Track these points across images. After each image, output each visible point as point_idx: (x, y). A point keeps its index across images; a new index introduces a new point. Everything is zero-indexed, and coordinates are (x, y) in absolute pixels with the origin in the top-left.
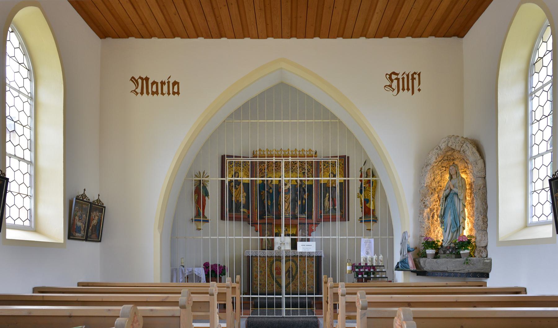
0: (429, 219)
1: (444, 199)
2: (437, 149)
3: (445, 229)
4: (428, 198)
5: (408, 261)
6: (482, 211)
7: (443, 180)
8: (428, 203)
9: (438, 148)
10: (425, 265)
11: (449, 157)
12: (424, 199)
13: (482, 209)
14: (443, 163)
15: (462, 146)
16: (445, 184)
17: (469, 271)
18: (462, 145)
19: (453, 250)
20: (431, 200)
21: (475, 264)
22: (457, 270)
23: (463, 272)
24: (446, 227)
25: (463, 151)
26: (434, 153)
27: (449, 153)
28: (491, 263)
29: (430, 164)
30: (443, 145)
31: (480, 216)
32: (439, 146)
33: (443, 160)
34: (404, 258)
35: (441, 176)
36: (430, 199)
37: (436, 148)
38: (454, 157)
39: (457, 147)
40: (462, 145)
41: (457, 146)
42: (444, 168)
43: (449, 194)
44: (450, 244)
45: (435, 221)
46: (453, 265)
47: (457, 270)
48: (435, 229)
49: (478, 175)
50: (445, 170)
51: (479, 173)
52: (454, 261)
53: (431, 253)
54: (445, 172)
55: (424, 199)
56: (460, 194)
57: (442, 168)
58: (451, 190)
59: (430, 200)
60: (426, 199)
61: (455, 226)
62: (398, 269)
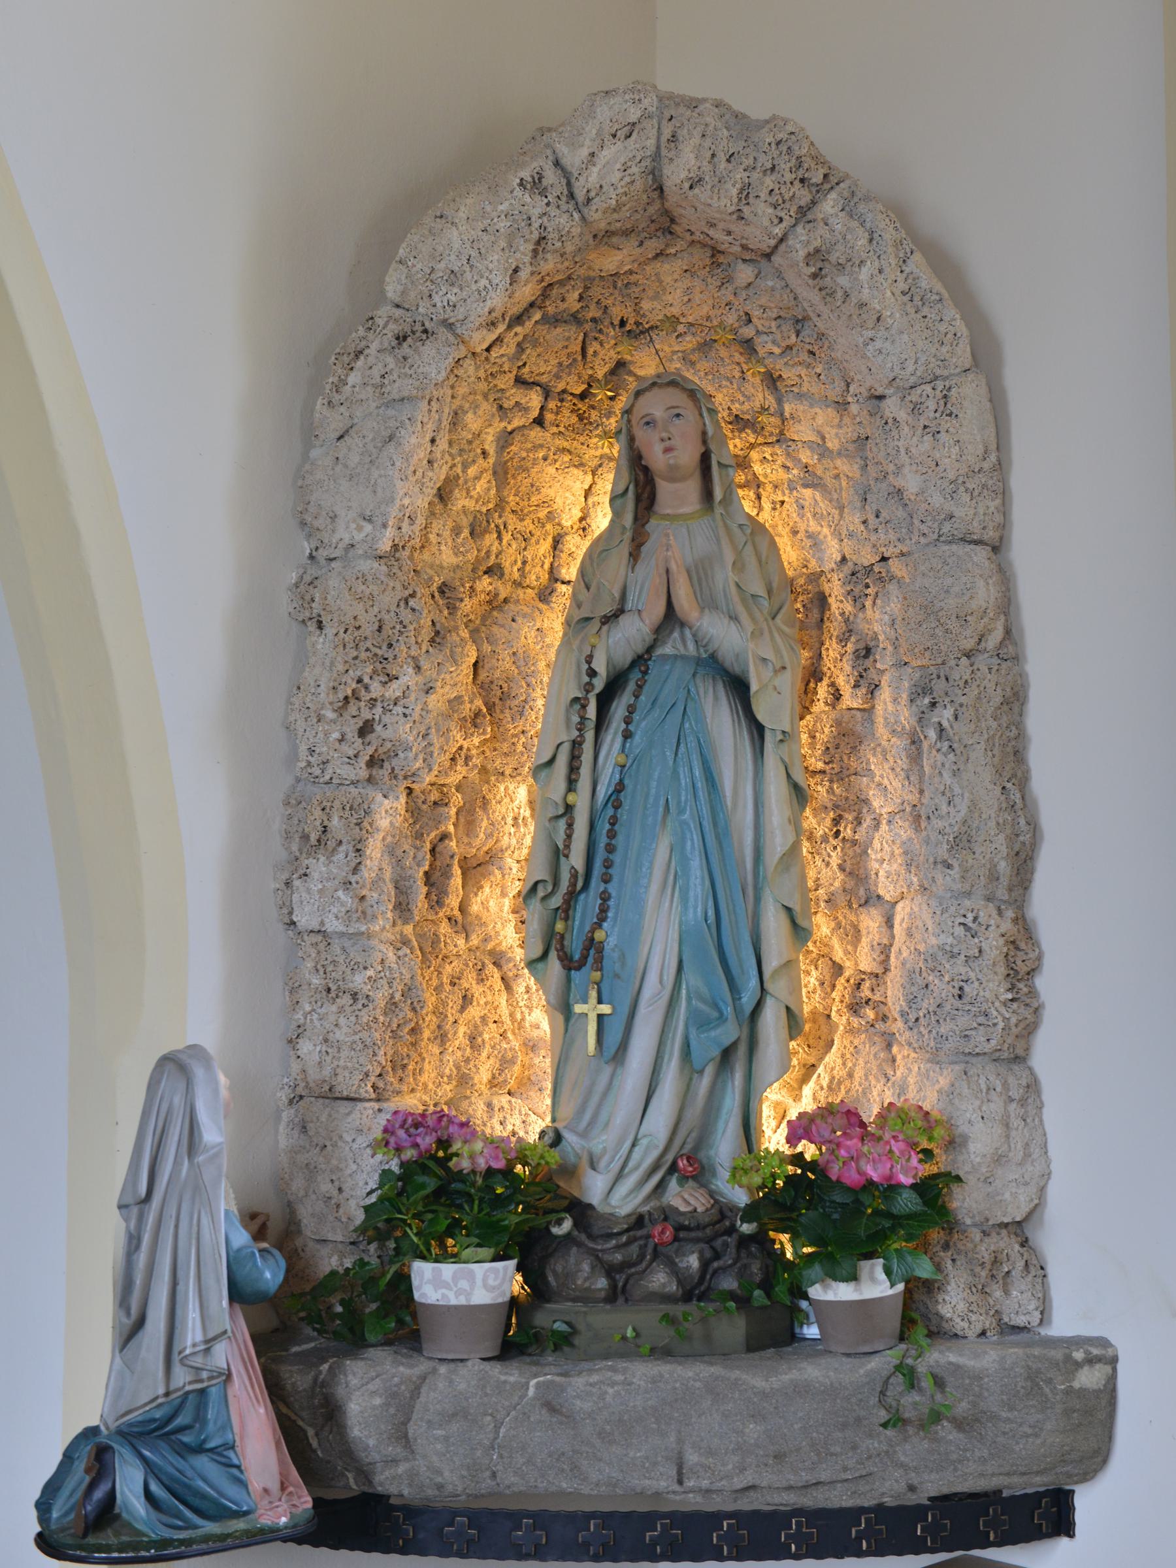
0: (403, 908)
1: (592, 711)
2: (536, 184)
3: (613, 1037)
4: (408, 677)
5: (227, 1425)
6: (1003, 864)
7: (520, 514)
8: (404, 731)
9: (551, 177)
10: (402, 1436)
11: (596, 291)
12: (376, 689)
13: (1004, 850)
14: (536, 344)
15: (803, 211)
16: (528, 555)
17: (912, 1488)
18: (804, 197)
19: (717, 1256)
20: (432, 698)
21: (994, 1417)
22: (790, 1488)
23: (848, 1503)
24: (625, 1010)
25: (816, 255)
26: (503, 224)
27: (618, 257)
28: (1109, 1393)
29: (450, 326)
30: (605, 155)
31: (987, 913)
32: (557, 163)
33: (537, 316)
34: (181, 1378)
35: (501, 474)
36: (429, 690)
37: (526, 174)
38: (646, 305)
39: (762, 212)
40: (804, 197)
41: (763, 195)
42: (534, 399)
43: (641, 661)
44: (661, 1186)
45: (444, 928)
46: (753, 1431)
47: (790, 1488)
48: (452, 1012)
49: (959, 512)
50: (539, 421)
51: (966, 498)
52: (764, 1395)
53: (481, 1297)
54: (536, 433)
55: (376, 689)
56: (767, 673)
57: (516, 395)
58: (671, 617)
59: (425, 709)
60: (394, 690)
61: (716, 1006)
62: (108, 1537)
